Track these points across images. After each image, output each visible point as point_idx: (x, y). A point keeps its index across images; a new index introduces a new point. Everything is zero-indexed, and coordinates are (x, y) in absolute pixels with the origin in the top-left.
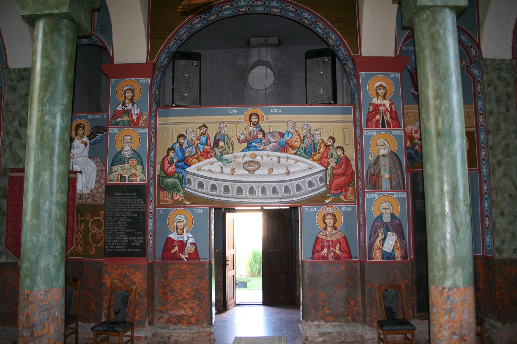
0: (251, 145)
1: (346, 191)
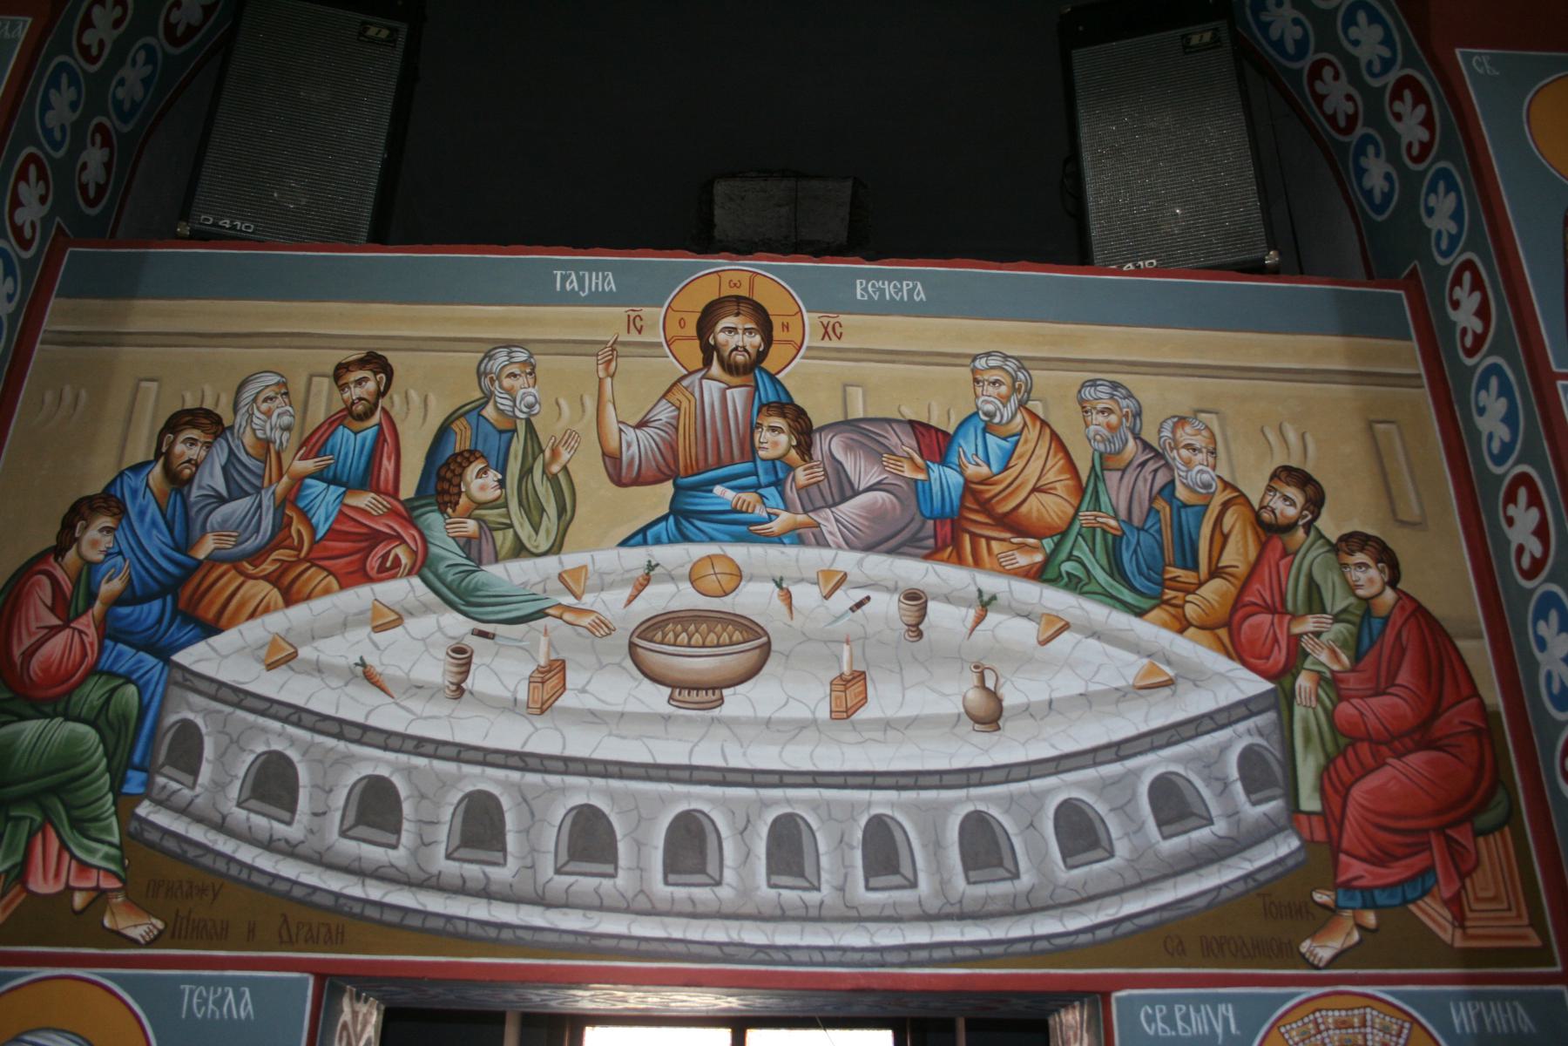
0: (704, 503)
1: (1463, 866)
